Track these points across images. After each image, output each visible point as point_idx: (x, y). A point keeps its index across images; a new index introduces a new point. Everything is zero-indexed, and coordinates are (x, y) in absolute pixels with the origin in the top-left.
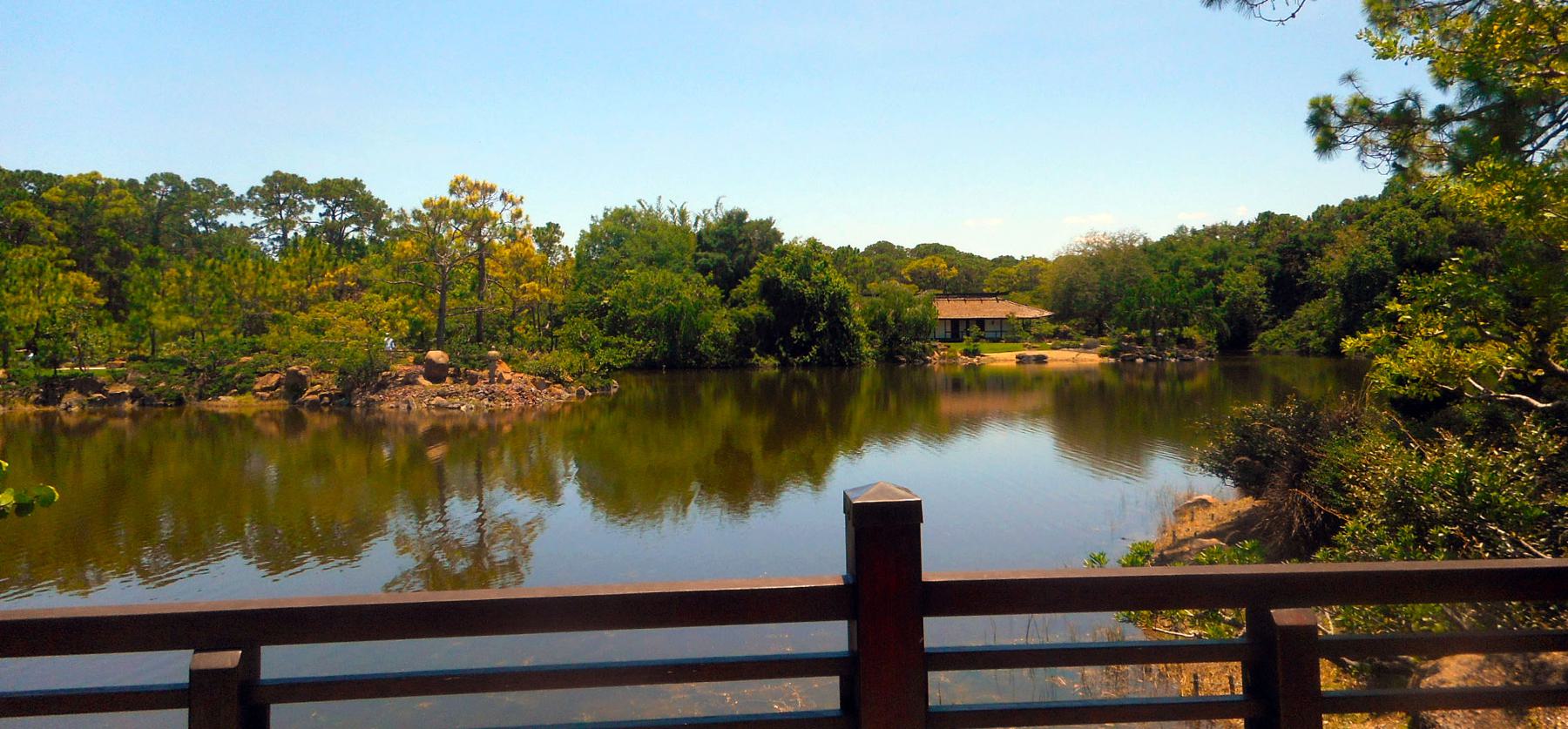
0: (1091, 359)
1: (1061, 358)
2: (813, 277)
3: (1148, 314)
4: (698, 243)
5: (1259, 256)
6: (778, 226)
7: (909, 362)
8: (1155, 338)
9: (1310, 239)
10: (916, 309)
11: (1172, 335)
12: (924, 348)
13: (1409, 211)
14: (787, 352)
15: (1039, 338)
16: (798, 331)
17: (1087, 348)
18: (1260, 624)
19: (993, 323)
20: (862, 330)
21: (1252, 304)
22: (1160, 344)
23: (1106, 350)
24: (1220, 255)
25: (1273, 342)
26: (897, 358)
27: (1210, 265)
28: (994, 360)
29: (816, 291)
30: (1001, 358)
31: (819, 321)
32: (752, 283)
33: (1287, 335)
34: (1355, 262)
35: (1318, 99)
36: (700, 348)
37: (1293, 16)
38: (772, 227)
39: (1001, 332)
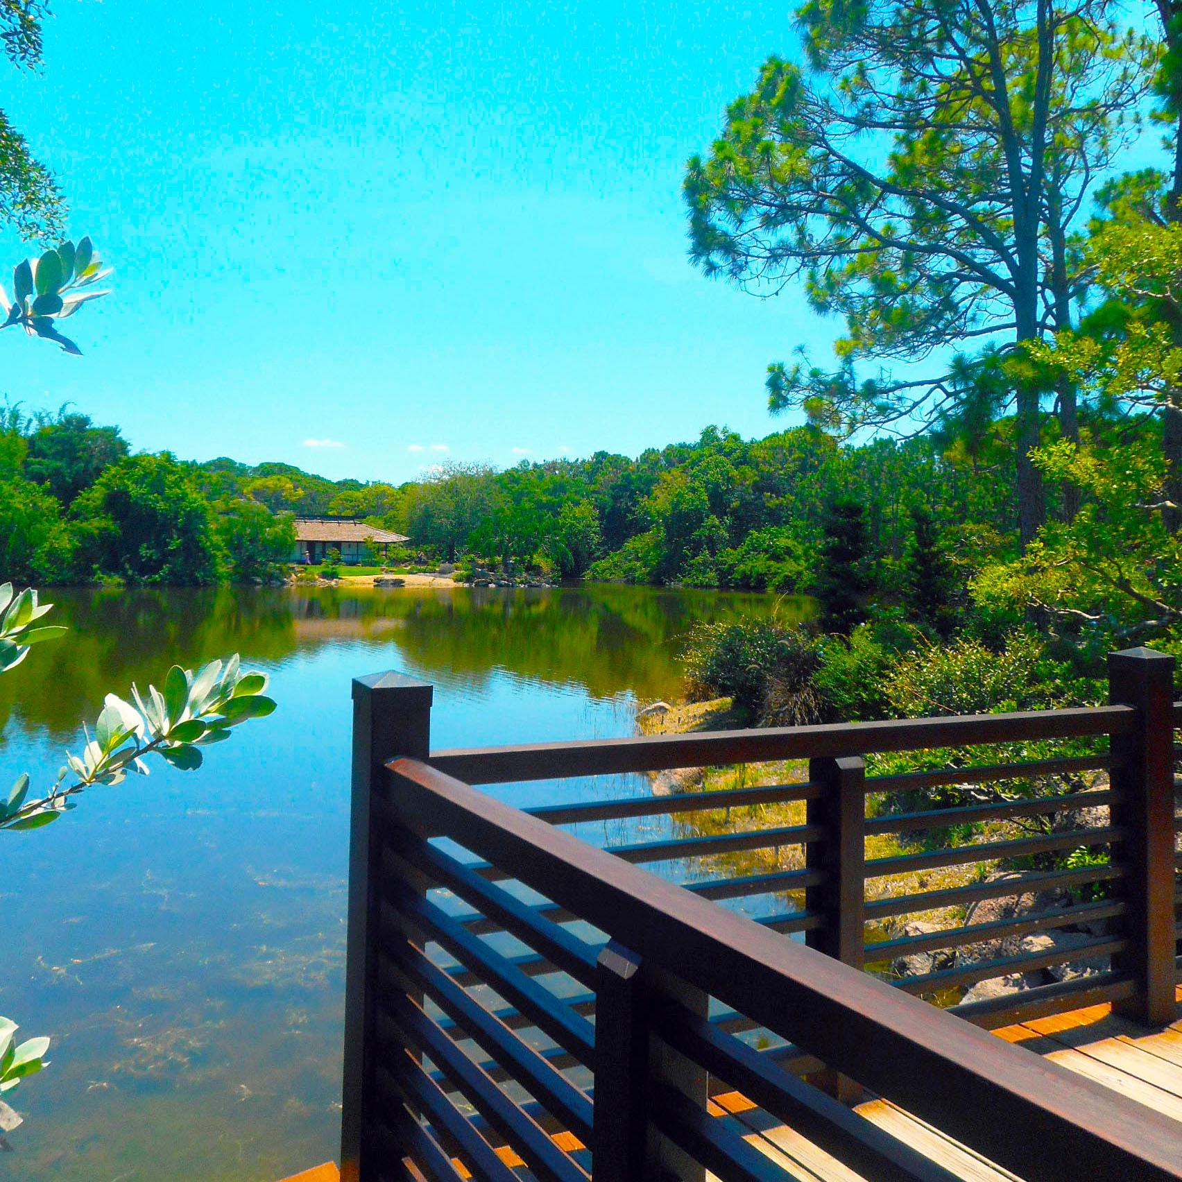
0: (446, 583)
1: (418, 582)
2: (167, 491)
3: (502, 542)
4: (29, 448)
5: (594, 492)
6: (123, 435)
7: (265, 583)
8: (506, 565)
9: (640, 479)
10: (276, 529)
11: (522, 562)
12: (280, 569)
13: (723, 458)
14: (134, 571)
15: (396, 562)
16: (148, 548)
17: (442, 572)
18: (823, 770)
19: (349, 546)
20: (219, 549)
21: (586, 537)
22: (511, 571)
23: (461, 575)
24: (559, 488)
25: (604, 571)
26: (253, 580)
27: (549, 498)
28: (352, 583)
29: (170, 506)
30: (359, 581)
31: (172, 538)
32: (95, 495)
33: (616, 566)
34: (678, 500)
35: (774, 365)
36: (33, 564)
37: (777, 294)
38: (118, 436)
39: (361, 555)
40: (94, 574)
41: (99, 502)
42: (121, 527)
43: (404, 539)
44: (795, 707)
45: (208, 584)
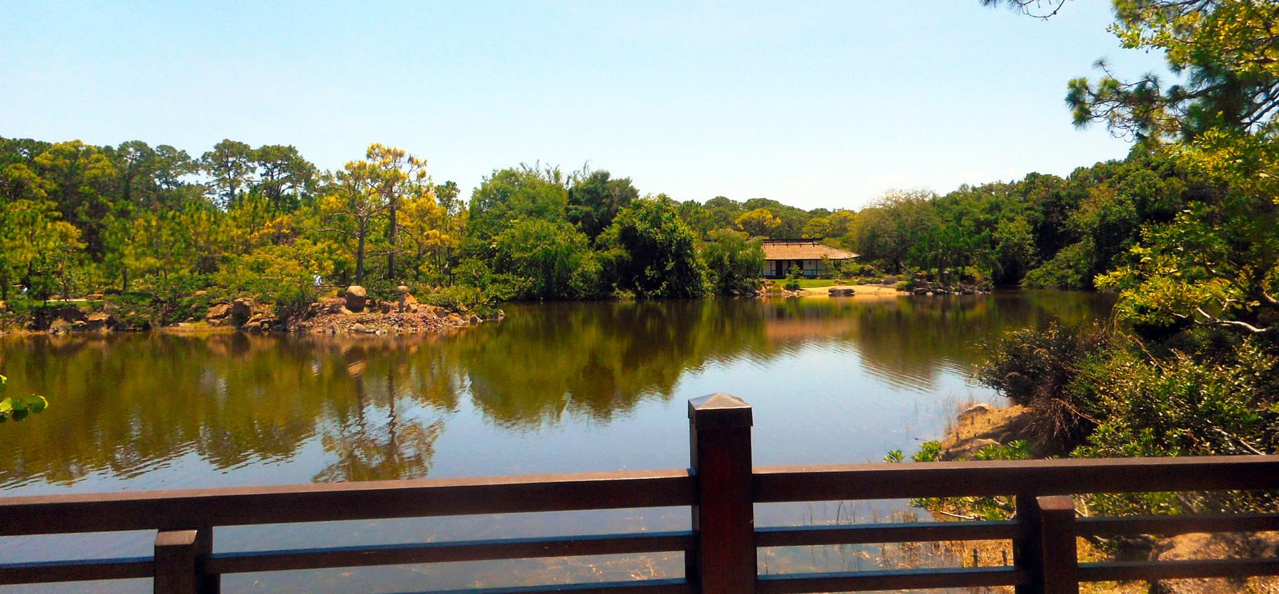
0: (890, 293)
1: (866, 292)
3: (936, 256)
5: (1027, 209)
6: (633, 184)
7: (741, 295)
8: (942, 276)
9: (1069, 195)
12: (753, 284)
13: (1149, 172)
15: (848, 275)
16: (651, 270)
17: (887, 283)
21: (1021, 248)
22: (946, 280)
24: (995, 208)
27: (987, 216)
28: (811, 293)
30: (816, 292)
31: (668, 262)
32: (614, 231)
33: (1050, 273)
35: (1075, 81)
36: (571, 283)
37: (1055, 13)
39: (816, 270)
40: (613, 290)
41: (616, 236)
42: (631, 254)
43: (854, 255)
44: (1055, 414)
45: (697, 297)
